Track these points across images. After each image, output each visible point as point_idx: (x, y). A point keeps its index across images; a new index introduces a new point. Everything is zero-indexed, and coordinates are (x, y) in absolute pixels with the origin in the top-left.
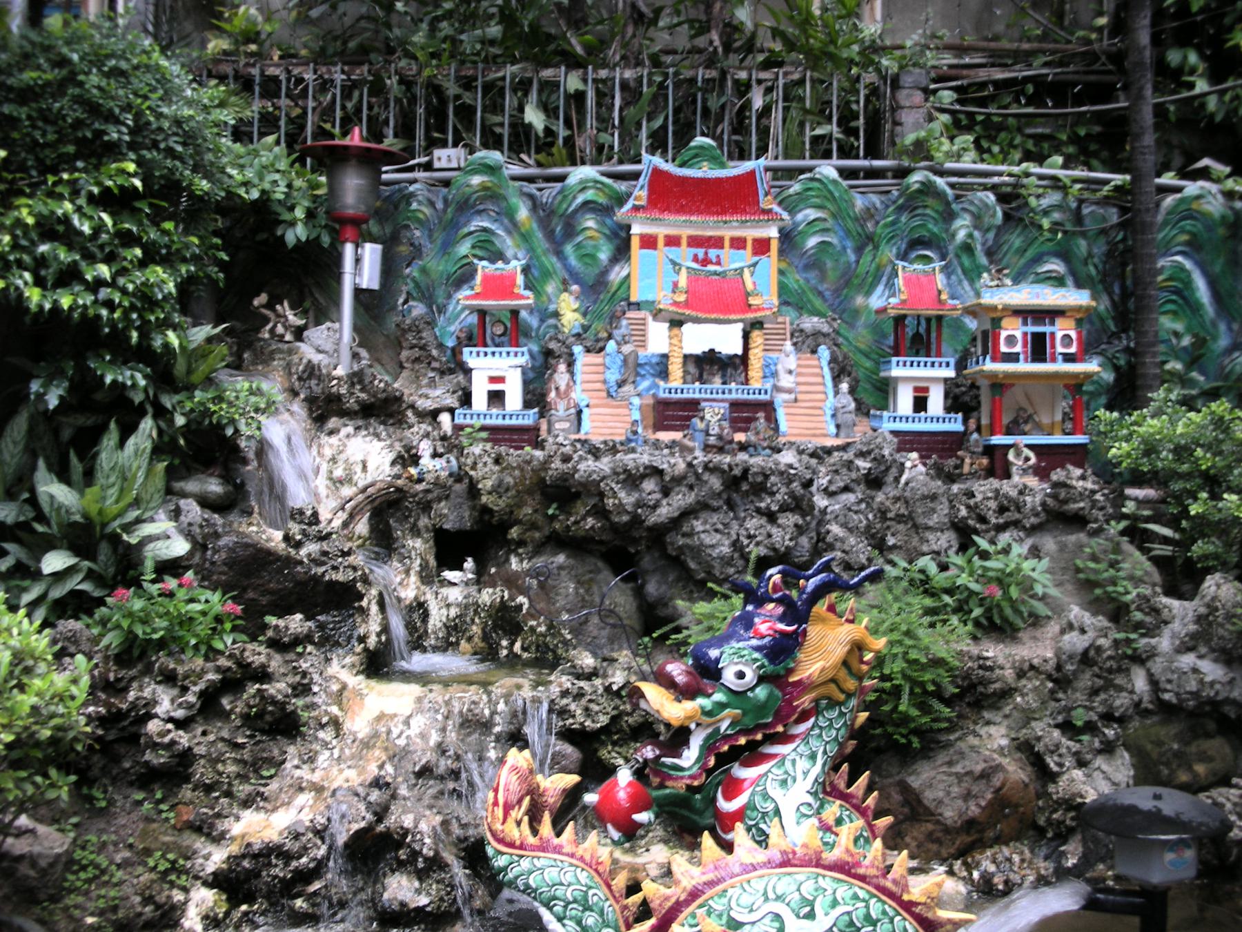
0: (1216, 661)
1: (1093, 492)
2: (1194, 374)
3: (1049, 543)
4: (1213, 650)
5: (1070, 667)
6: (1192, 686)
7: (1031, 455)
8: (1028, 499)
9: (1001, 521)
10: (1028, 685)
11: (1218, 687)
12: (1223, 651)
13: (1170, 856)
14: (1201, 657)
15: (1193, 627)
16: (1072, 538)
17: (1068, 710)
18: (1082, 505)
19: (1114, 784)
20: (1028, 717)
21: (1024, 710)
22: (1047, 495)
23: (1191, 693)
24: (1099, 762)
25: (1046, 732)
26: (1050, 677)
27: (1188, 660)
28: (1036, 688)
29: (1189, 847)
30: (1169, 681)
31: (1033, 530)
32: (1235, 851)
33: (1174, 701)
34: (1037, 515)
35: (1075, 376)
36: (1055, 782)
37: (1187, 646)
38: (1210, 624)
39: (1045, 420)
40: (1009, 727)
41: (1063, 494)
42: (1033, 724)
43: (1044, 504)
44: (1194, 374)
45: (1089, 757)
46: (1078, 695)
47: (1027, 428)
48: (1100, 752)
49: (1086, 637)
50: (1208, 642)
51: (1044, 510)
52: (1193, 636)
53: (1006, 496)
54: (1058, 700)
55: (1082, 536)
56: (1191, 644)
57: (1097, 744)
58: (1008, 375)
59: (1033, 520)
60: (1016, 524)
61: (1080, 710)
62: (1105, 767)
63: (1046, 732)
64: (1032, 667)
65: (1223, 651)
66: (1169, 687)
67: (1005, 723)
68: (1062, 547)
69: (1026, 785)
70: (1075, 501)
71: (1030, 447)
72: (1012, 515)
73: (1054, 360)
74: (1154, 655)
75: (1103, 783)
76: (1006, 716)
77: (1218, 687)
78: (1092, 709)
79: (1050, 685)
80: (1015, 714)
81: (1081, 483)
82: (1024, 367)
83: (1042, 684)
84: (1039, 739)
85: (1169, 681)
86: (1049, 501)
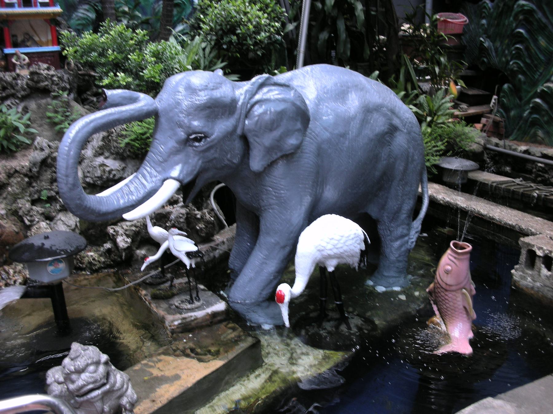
0: (115, 159)
1: (53, 76)
2: (137, 13)
3: (33, 105)
4: (112, 154)
5: (35, 170)
6: (98, 173)
7: (27, 58)
8: (19, 82)
9: (4, 95)
10: (14, 181)
11: (114, 172)
12: (117, 154)
13: (50, 268)
14: (106, 158)
15: (101, 143)
16: (43, 101)
17: (39, 192)
18: (46, 83)
19: (68, 226)
20: (15, 198)
21: (12, 195)
22: (29, 79)
23: (98, 177)
24: (61, 216)
25: (24, 204)
26: (26, 175)
27: (100, 160)
28: (18, 182)
29: (61, 262)
30: (88, 172)
31: (23, 98)
32: (124, 254)
33: (92, 182)
34: (24, 90)
35: (48, 14)
36: (30, 230)
37: (99, 153)
38: (109, 141)
39: (44, 40)
40: (7, 204)
41: (36, 78)
42: (19, 201)
43: (27, 84)
44: (137, 13)
45: (54, 214)
46: (44, 183)
47: (28, 44)
48: (60, 211)
49: (43, 153)
50: (109, 150)
51: (28, 87)
52: (101, 148)
53: (6, 82)
54: (33, 187)
55: (49, 100)
56: (100, 152)
57: (58, 207)
58: (8, 15)
59: (23, 93)
60: (13, 96)
61: (45, 191)
62: (63, 218)
63: (24, 204)
64: (16, 171)
65: (117, 154)
66: (88, 175)
67: (5, 202)
68: (39, 106)
69: (17, 233)
70: (43, 81)
71: (26, 54)
72: (10, 91)
73: (36, 6)
74: (84, 159)
75: (62, 226)
76: (5, 198)
77: (114, 172)
78: (52, 190)
79: (26, 179)
80: (9, 197)
81: (46, 72)
82: (18, 10)
83: (22, 179)
84: (20, 208)
85: (88, 172)
86: (29, 82)
